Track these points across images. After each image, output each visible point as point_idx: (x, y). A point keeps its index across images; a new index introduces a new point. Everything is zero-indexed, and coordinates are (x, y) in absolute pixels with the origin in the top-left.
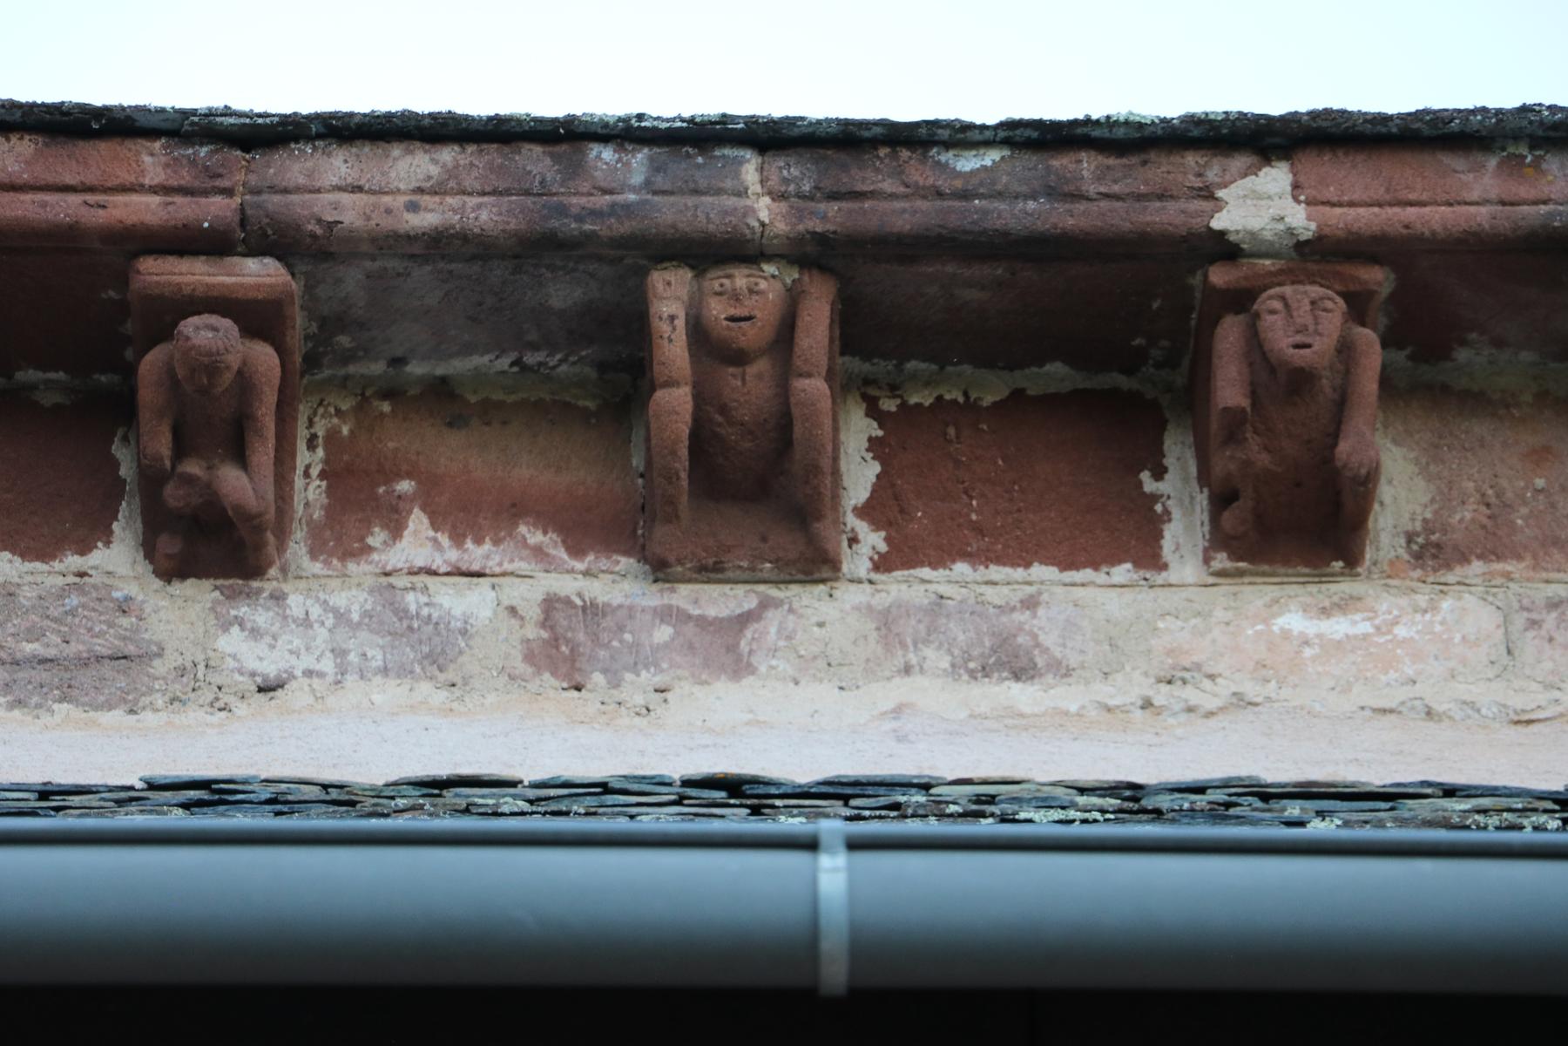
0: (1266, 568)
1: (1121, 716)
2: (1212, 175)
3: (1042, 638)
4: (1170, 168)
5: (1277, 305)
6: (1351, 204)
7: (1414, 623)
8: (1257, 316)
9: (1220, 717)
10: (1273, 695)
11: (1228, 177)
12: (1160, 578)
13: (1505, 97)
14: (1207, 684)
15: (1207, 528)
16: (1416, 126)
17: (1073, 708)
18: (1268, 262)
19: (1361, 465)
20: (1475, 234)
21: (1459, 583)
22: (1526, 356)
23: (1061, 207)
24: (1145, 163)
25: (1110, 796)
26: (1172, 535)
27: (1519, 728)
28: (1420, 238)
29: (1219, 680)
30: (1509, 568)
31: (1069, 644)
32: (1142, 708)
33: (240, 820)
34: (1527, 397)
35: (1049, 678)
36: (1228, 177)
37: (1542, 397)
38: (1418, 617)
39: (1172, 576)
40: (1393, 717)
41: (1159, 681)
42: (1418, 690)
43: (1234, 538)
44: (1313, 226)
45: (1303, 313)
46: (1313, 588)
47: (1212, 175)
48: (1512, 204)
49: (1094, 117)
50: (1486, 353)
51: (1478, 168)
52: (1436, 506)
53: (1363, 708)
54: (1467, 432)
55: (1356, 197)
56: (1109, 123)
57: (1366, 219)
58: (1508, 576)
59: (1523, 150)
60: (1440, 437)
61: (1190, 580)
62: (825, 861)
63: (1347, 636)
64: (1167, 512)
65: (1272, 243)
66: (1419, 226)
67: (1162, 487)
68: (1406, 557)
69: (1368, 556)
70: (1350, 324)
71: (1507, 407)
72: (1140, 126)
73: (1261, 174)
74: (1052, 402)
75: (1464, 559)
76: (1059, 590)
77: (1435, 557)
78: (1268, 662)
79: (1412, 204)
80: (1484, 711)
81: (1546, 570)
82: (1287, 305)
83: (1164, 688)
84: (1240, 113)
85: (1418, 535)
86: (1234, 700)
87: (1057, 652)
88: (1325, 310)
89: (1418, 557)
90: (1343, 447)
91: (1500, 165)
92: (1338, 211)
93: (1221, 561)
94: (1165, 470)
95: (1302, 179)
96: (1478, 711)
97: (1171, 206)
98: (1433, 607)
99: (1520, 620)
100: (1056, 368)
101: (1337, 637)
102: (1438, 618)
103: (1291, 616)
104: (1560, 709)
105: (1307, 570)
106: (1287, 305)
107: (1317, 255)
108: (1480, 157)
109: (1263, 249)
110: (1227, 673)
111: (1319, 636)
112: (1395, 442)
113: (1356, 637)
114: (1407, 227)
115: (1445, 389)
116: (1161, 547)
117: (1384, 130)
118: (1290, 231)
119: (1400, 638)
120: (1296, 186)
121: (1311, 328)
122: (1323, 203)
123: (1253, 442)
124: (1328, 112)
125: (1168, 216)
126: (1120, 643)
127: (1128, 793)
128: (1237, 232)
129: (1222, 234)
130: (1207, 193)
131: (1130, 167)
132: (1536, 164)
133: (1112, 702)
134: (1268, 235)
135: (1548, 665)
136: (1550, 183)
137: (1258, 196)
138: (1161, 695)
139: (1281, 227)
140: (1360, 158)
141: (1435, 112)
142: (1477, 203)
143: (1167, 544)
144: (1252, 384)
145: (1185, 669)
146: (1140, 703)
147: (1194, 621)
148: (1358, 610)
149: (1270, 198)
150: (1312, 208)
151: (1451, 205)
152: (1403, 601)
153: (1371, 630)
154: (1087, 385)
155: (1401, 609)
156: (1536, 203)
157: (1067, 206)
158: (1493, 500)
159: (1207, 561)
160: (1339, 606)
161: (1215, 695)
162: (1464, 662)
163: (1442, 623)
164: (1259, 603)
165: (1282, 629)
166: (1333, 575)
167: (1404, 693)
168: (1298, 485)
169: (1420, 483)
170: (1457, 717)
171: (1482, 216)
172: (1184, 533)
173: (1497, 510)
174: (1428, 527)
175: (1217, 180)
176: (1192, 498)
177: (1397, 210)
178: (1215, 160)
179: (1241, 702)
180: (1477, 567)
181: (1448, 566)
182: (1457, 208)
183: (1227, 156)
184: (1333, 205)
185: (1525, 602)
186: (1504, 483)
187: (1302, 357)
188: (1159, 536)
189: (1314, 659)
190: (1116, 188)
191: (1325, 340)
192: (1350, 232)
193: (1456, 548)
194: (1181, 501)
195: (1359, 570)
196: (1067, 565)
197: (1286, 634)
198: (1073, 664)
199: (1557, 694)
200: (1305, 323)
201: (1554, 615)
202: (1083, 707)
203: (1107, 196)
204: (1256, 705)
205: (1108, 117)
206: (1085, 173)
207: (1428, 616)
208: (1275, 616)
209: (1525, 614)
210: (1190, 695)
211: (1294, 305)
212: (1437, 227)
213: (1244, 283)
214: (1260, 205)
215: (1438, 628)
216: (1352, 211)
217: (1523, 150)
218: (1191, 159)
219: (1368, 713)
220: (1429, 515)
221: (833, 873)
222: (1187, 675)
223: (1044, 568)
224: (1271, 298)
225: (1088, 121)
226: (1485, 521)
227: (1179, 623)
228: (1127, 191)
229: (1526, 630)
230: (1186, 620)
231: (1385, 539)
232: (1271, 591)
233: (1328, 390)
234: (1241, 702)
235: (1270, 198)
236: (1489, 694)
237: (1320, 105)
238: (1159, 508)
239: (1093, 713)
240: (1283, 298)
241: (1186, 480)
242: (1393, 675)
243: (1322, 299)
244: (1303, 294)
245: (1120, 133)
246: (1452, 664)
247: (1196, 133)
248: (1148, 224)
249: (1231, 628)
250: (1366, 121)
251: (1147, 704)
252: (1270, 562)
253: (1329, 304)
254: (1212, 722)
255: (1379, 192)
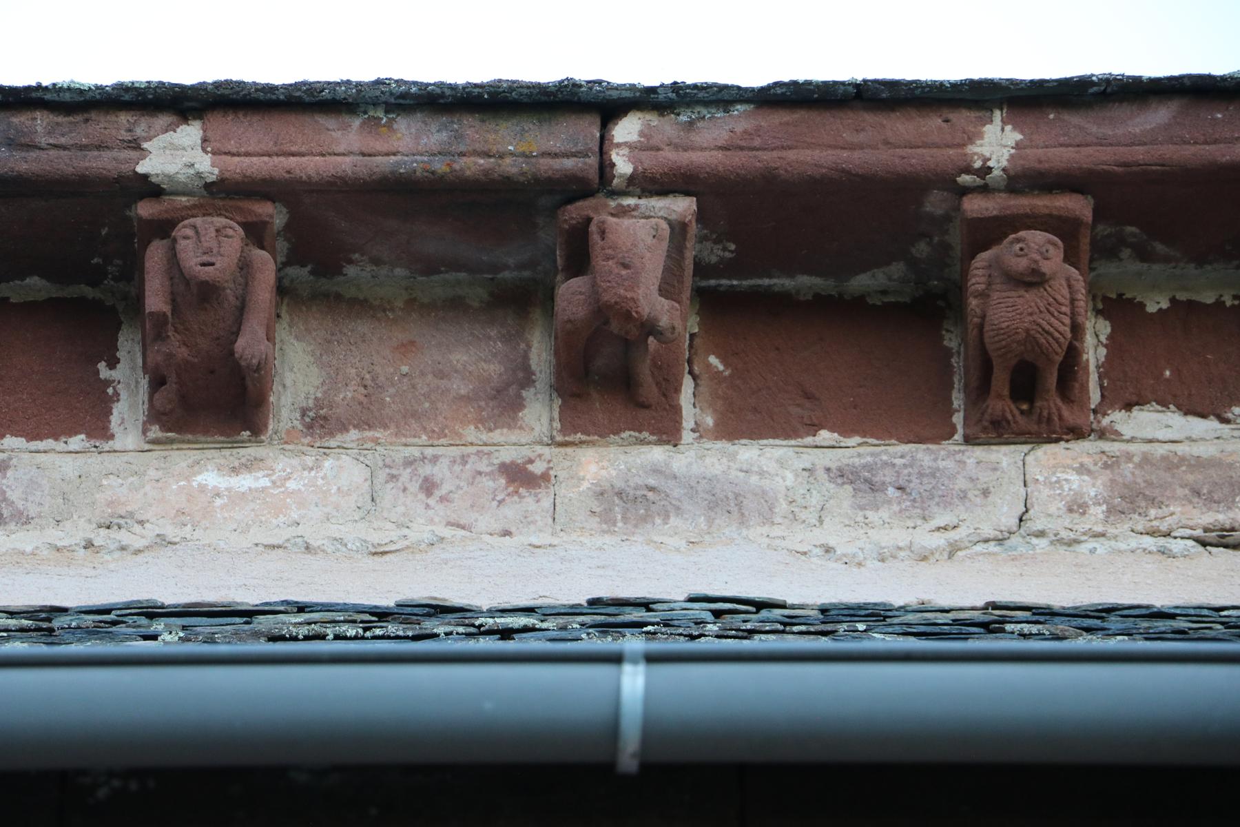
0: (190, 437)
1: (68, 554)
2: (139, 131)
3: (9, 493)
4: (107, 125)
5: (189, 232)
6: (247, 154)
7: (301, 478)
8: (175, 240)
9: (146, 554)
10: (188, 536)
11: (152, 133)
12: (110, 444)
13: (365, 74)
14: (137, 528)
15: (146, 406)
16: (298, 94)
17: (29, 549)
18: (184, 199)
19: (253, 357)
20: (341, 178)
21: (339, 447)
22: (399, 272)
23: (18, 155)
24: (87, 121)
25: (26, 618)
26: (119, 411)
27: (376, 558)
28: (299, 181)
29: (147, 525)
30: (378, 435)
31: (30, 499)
32: (85, 548)
33: (880, 641)
34: (399, 304)
35: (12, 526)
36: (152, 133)
37: (411, 303)
38: (306, 473)
39: (116, 444)
40: (280, 551)
41: (100, 527)
42: (300, 530)
43: (164, 414)
44: (216, 171)
45: (209, 239)
46: (227, 452)
47: (139, 131)
48: (370, 155)
49: (44, 84)
50: (368, 269)
51: (345, 128)
52: (325, 388)
53: (257, 545)
54: (352, 331)
55: (250, 149)
56: (55, 88)
57: (257, 166)
58: (376, 441)
59: (380, 113)
60: (332, 334)
61: (131, 447)
62: (627, 668)
63: (250, 489)
64: (117, 394)
65: (185, 184)
66: (298, 172)
67: (114, 374)
68: (300, 427)
69: (271, 427)
70: (251, 247)
71: (384, 311)
72: (81, 92)
73: (178, 130)
74: (31, 308)
75: (344, 429)
76: (26, 456)
77: (323, 427)
78: (186, 510)
79: (293, 155)
80: (349, 546)
81: (405, 436)
82: (197, 232)
83: (103, 532)
84: (161, 83)
85: (311, 410)
86: (158, 540)
87: (20, 505)
88: (226, 236)
89: (310, 427)
90: (240, 344)
91: (362, 126)
92: (236, 159)
93: (155, 432)
94: (118, 361)
95: (209, 134)
96: (346, 545)
97: (106, 155)
98: (317, 466)
99: (382, 475)
100: (34, 281)
101: (242, 490)
102: (321, 474)
103: (210, 475)
104: (407, 543)
105: (222, 438)
106: (197, 232)
107: (222, 193)
108: (347, 118)
109: (180, 189)
110: (153, 520)
111: (229, 489)
112: (297, 338)
113: (257, 490)
114: (289, 172)
115: (339, 297)
116: (110, 422)
117: (274, 97)
118: (199, 175)
119: (290, 490)
120: (205, 140)
121: (215, 251)
122: (226, 153)
123: (174, 338)
124: (228, 83)
125: (104, 163)
126: (71, 497)
127: (44, 615)
128: (157, 175)
129: (145, 177)
130: (135, 144)
131: (75, 124)
132: (389, 125)
133: (60, 544)
134: (182, 178)
135: (401, 509)
136: (399, 139)
137: (175, 147)
138: (100, 537)
139: (192, 171)
140: (255, 118)
141: (311, 84)
142: (344, 155)
143: (115, 419)
144: (172, 293)
145: (122, 517)
146: (83, 543)
147: (131, 479)
148: (260, 469)
149: (184, 149)
150: (217, 158)
151: (323, 155)
152: (295, 462)
153: (269, 484)
154: (60, 294)
155: (293, 467)
156: (387, 154)
157: (23, 154)
158: (369, 383)
159: (144, 432)
160: (246, 466)
161: (143, 537)
162: (337, 508)
163: (323, 479)
164: (184, 464)
165: (199, 485)
166: (243, 442)
167: (292, 531)
168: (212, 372)
169: (315, 370)
170: (329, 551)
171: (346, 165)
172: (128, 414)
173: (371, 389)
174: (319, 404)
175: (144, 134)
176: (137, 382)
177: (282, 159)
178: (143, 119)
179: (163, 542)
180: (354, 434)
181: (332, 434)
182: (328, 158)
183: (152, 116)
184: (234, 155)
185: (388, 461)
186: (378, 369)
187: (207, 273)
188: (109, 412)
189: (222, 507)
190: (63, 140)
191: (226, 259)
192: (245, 176)
193: (338, 419)
194: (128, 385)
195: (263, 438)
196: (31, 437)
197: (202, 488)
198: (32, 514)
199: (406, 531)
200: (211, 246)
201: (409, 470)
202: (37, 548)
203: (55, 146)
204: (175, 544)
205: (54, 85)
206: (39, 129)
207: (313, 473)
208: (195, 474)
209: (387, 470)
210: (124, 537)
211: (202, 232)
212: (312, 173)
213: (166, 216)
214: (176, 154)
215: (320, 482)
216: (247, 160)
217: (380, 114)
218: (124, 118)
219: (261, 548)
220: (319, 395)
221: (633, 681)
222: (122, 521)
223: (14, 439)
224: (185, 227)
225: (39, 87)
226: (362, 398)
227: (120, 481)
228: (72, 142)
229: (387, 482)
230: (125, 478)
231: (285, 413)
232: (194, 455)
233: (231, 298)
234: (163, 542)
235: (184, 149)
236: (354, 533)
237: (222, 76)
238: (110, 391)
239: (45, 553)
240: (194, 227)
241: (133, 369)
242: (282, 518)
243: (225, 227)
244: (208, 224)
245: (67, 97)
246: (326, 510)
247: (127, 97)
248: (87, 169)
249: (160, 485)
250: (257, 90)
251: (89, 545)
252: (193, 432)
253: (230, 232)
254: (140, 558)
255: (270, 146)
